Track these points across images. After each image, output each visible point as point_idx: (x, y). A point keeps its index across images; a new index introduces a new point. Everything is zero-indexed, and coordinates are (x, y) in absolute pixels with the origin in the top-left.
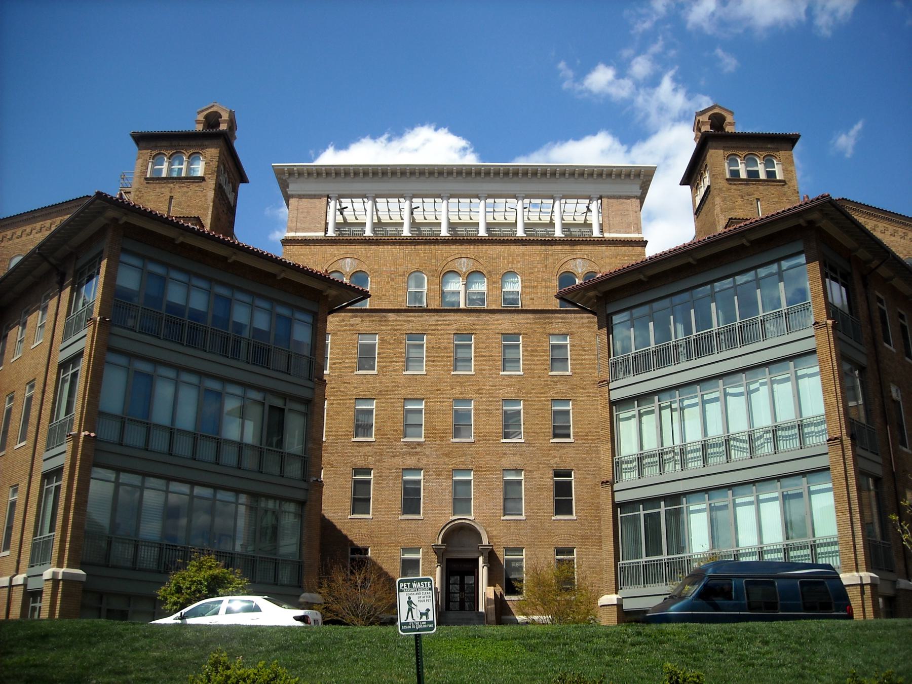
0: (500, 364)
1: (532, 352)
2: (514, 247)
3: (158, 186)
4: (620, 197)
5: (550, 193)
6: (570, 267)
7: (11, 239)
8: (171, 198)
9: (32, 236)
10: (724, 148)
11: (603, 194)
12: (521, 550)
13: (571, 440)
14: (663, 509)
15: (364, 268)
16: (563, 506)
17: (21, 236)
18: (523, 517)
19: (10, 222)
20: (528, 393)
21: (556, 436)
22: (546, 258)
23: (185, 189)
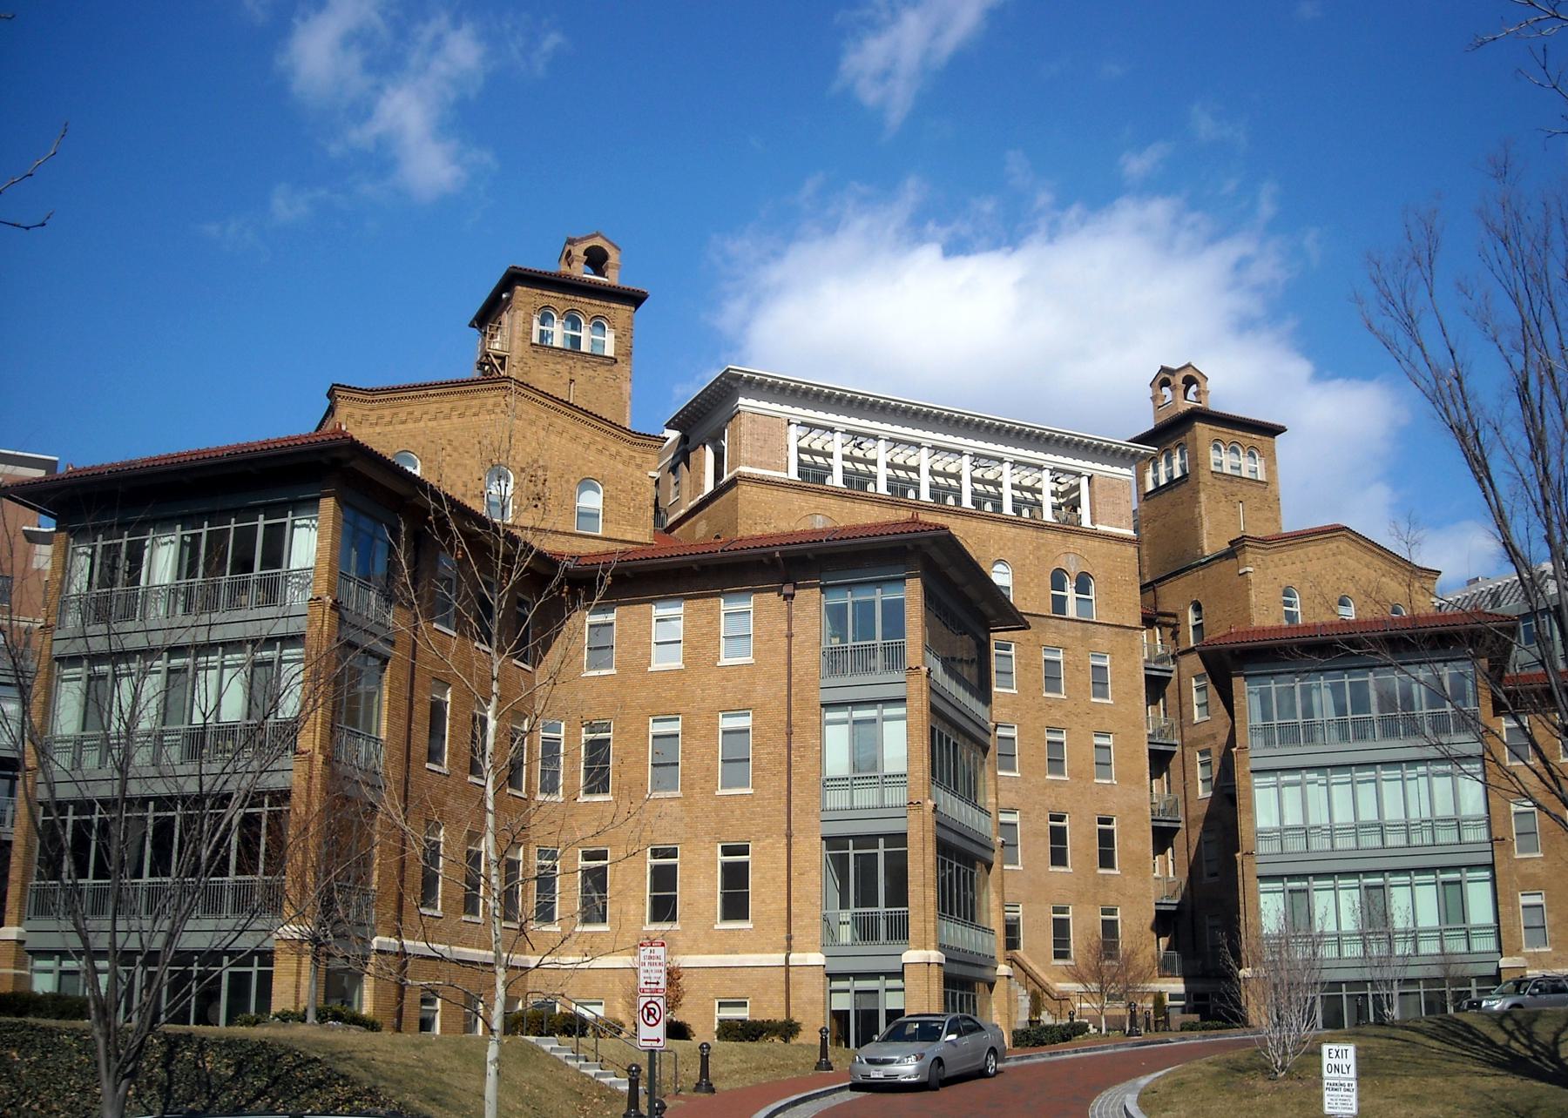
1: (1025, 667)
9: (422, 424)
16: (1058, 858)
22: (1038, 548)
23: (590, 373)
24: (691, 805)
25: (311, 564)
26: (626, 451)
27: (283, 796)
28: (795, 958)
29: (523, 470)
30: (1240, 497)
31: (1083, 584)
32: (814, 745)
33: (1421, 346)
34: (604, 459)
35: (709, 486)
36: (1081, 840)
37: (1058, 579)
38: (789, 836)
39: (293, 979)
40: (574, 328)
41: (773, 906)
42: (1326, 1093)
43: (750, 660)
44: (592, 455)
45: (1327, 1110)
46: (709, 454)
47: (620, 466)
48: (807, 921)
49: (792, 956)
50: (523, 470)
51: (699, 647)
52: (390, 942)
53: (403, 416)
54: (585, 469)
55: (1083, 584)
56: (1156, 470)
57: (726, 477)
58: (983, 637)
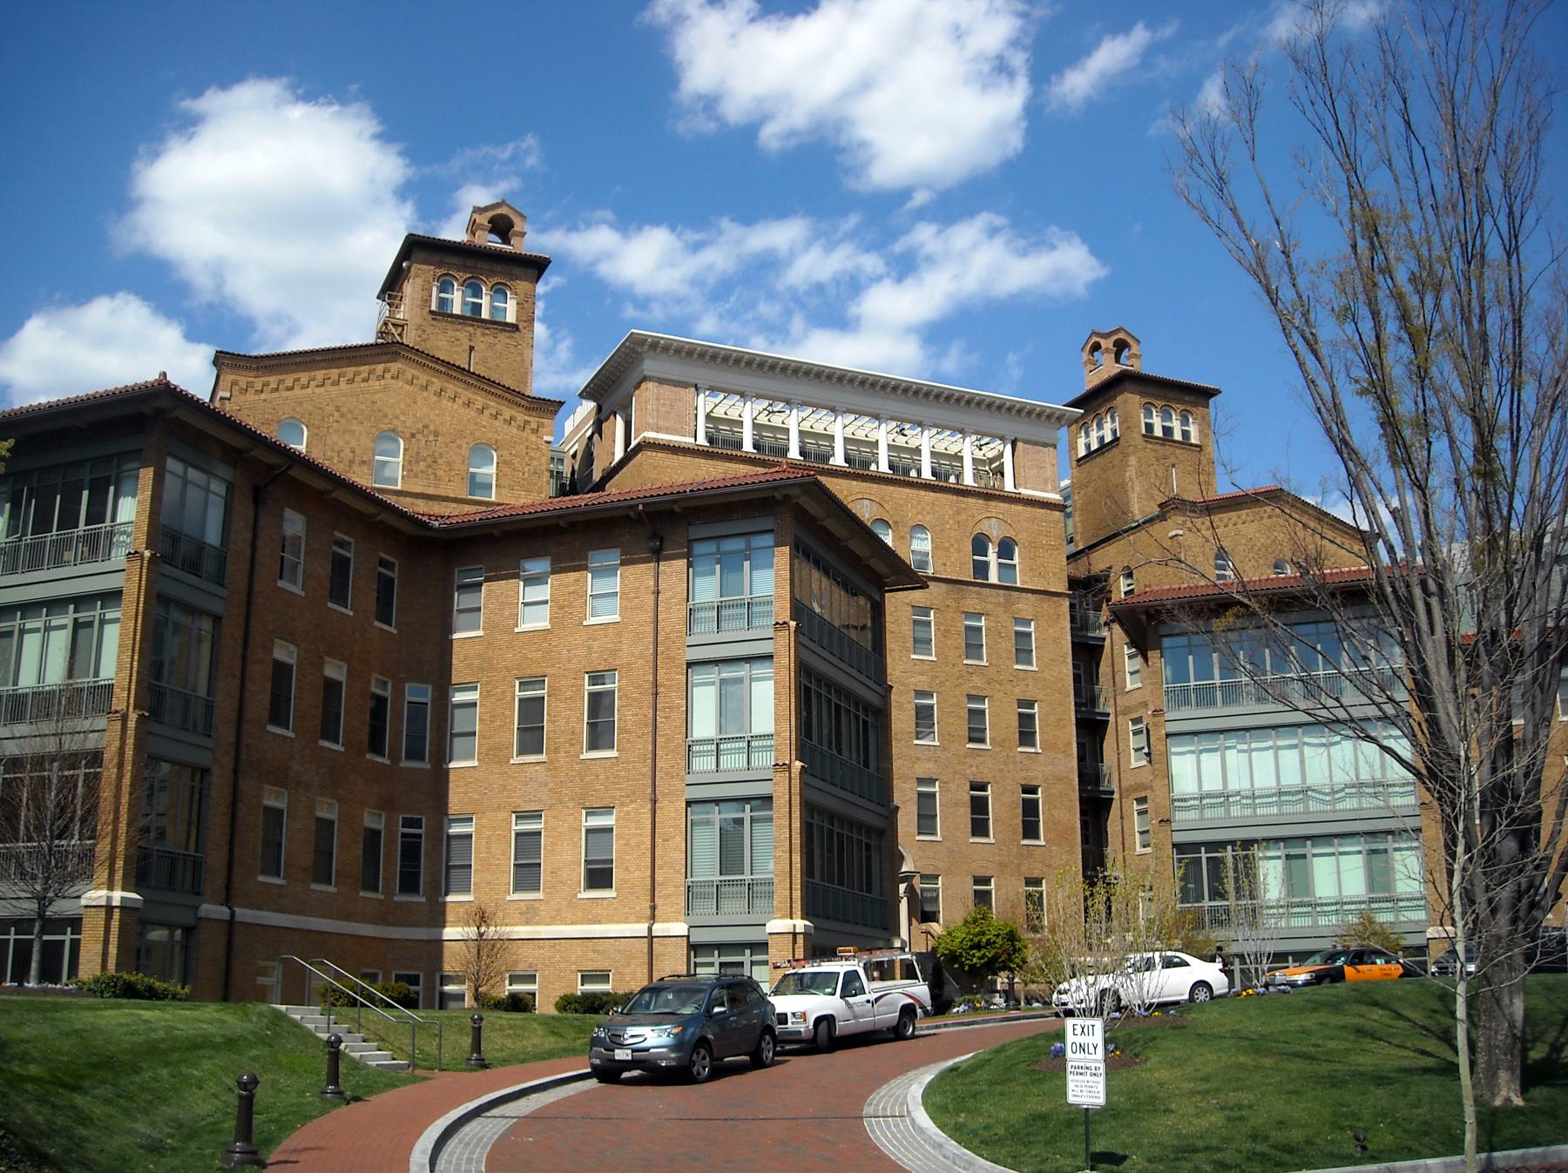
0: (910, 644)
1: (945, 634)
2: (922, 493)
3: (449, 326)
4: (1036, 443)
5: (831, 404)
6: (984, 527)
7: (277, 390)
8: (472, 348)
9: (309, 391)
10: (1142, 394)
11: (1019, 436)
12: (936, 877)
13: (988, 747)
14: (1229, 853)
15: (1011, 534)
16: (980, 828)
17: (292, 388)
18: (939, 838)
19: (275, 362)
20: (942, 684)
21: (971, 740)
22: (958, 513)
23: (491, 339)
24: (556, 769)
25: (133, 518)
26: (521, 417)
27: (96, 758)
28: (658, 929)
29: (413, 435)
30: (1172, 460)
31: (1006, 549)
32: (679, 707)
33: (1234, 210)
34: (497, 423)
35: (619, 454)
36: (1003, 809)
37: (980, 545)
38: (654, 801)
39: (100, 947)
40: (475, 296)
41: (637, 874)
42: (1070, 1077)
43: (616, 618)
44: (485, 419)
45: (1071, 1099)
46: (620, 422)
47: (515, 431)
48: (672, 889)
49: (656, 926)
50: (413, 435)
51: (563, 611)
52: (221, 912)
53: (289, 383)
54: (478, 434)
55: (1006, 549)
56: (1087, 435)
57: (634, 443)
58: (878, 598)
